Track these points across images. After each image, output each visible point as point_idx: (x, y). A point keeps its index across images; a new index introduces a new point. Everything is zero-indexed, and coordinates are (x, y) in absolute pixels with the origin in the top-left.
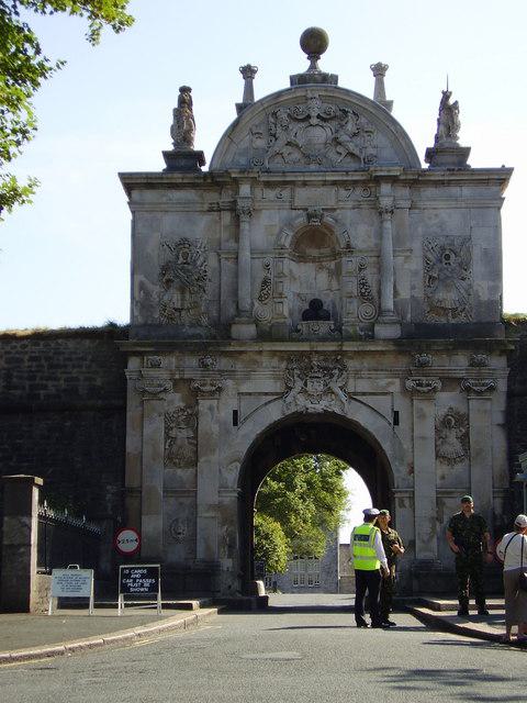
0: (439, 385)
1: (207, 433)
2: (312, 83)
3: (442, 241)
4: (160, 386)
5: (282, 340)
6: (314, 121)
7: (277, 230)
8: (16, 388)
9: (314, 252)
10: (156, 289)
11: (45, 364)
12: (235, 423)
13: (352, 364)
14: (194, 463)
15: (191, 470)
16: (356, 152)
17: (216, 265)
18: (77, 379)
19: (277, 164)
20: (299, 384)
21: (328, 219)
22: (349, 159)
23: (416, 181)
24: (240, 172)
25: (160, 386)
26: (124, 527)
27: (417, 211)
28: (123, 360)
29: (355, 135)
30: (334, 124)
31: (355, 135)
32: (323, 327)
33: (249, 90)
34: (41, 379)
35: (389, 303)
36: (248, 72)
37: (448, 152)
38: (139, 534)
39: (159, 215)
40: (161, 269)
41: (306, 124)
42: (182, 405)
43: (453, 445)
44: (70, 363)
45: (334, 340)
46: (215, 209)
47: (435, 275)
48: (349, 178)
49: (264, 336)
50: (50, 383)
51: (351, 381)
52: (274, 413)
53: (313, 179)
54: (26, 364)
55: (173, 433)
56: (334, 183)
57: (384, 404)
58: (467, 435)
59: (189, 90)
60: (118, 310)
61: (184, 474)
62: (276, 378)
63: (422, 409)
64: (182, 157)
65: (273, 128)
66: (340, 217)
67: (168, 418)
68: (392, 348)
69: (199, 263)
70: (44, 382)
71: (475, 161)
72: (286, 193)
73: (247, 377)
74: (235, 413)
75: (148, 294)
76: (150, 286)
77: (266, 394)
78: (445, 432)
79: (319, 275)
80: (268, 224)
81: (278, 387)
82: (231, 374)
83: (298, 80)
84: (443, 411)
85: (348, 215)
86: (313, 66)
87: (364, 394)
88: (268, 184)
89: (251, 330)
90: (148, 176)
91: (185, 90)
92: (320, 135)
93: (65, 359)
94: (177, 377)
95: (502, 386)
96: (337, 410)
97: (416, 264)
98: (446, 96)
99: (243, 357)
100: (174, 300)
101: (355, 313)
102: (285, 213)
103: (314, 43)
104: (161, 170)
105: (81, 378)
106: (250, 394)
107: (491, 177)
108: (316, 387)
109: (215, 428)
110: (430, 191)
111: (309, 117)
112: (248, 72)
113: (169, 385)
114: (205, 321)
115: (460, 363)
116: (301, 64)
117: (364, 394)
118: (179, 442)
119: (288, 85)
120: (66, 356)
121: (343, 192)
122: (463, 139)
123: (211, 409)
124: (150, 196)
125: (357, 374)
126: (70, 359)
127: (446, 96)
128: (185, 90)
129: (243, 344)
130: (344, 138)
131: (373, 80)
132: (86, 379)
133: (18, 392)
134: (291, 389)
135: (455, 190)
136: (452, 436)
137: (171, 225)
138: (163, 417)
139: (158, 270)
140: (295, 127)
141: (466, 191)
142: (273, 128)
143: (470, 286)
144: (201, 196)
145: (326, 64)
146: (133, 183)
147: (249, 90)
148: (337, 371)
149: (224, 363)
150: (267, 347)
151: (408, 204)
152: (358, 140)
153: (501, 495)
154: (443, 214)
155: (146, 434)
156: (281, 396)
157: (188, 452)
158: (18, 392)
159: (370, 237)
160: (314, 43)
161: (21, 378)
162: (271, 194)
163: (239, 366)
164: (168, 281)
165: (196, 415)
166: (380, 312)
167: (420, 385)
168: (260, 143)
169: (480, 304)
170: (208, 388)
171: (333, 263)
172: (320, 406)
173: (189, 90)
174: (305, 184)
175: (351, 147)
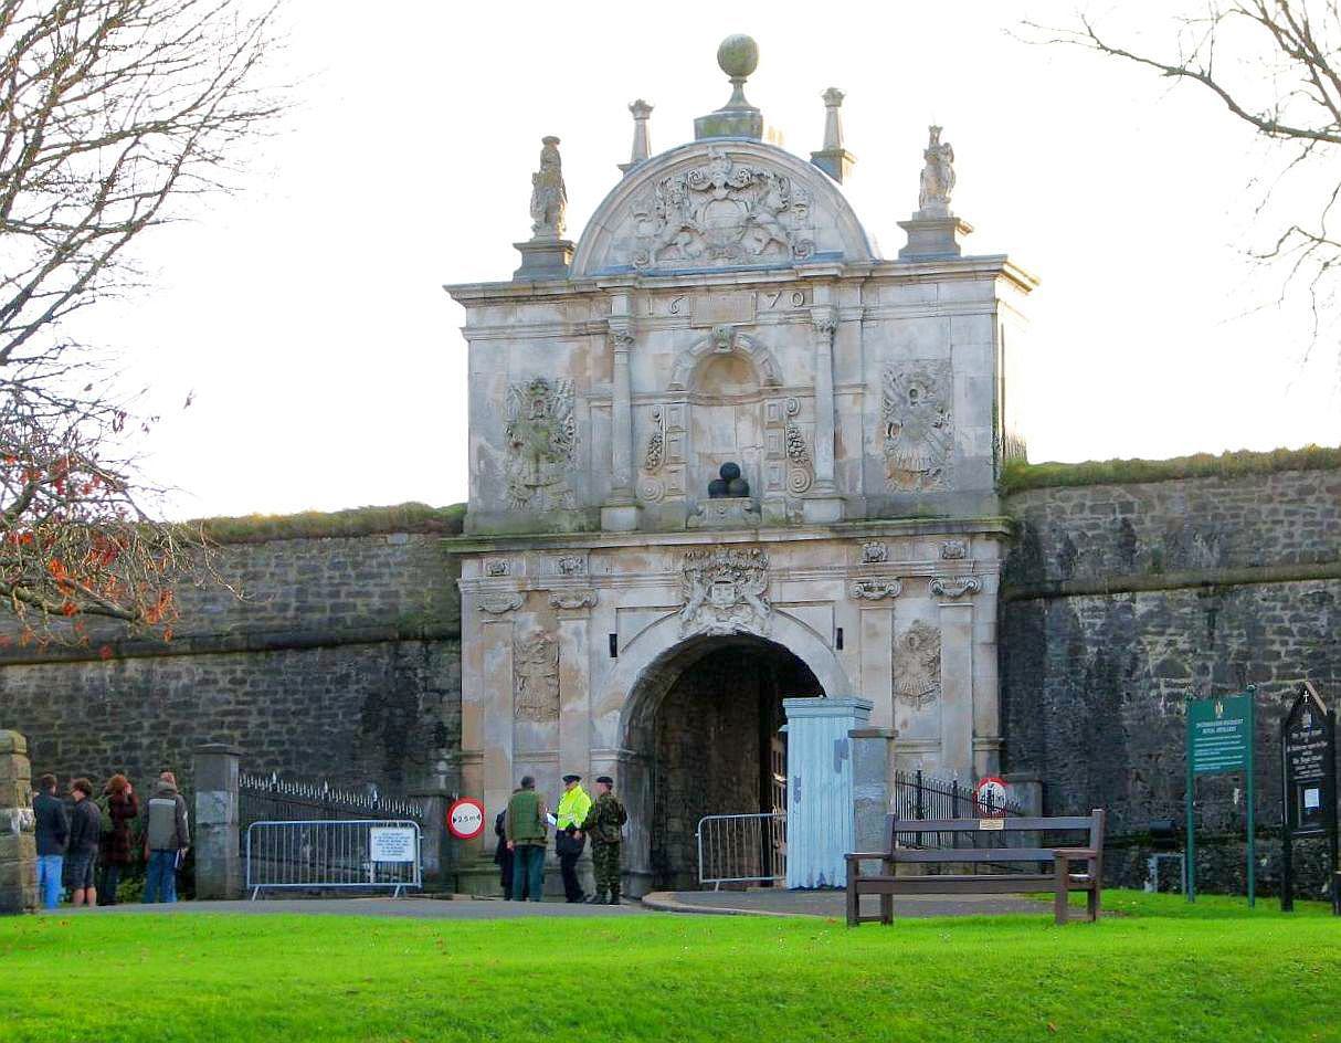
0: (896, 587)
1: (571, 669)
2: (734, 125)
3: (908, 369)
4: (505, 602)
5: (671, 530)
6: (721, 193)
7: (670, 362)
8: (311, 609)
9: (732, 389)
10: (501, 456)
11: (353, 574)
12: (614, 652)
13: (778, 561)
14: (556, 713)
15: (552, 724)
16: (781, 237)
17: (587, 418)
18: (396, 594)
19: (671, 262)
20: (699, 593)
21: (743, 344)
22: (773, 248)
23: (871, 276)
24: (610, 280)
25: (505, 602)
26: (463, 798)
27: (873, 323)
28: (456, 561)
29: (780, 211)
30: (747, 196)
31: (780, 211)
32: (735, 507)
33: (641, 139)
34: (349, 594)
35: (824, 468)
36: (641, 110)
37: (933, 233)
38: (482, 811)
39: (504, 344)
40: (523, 425)
41: (708, 197)
42: (538, 629)
43: (916, 674)
44: (386, 570)
45: (747, 527)
46: (582, 332)
47: (897, 422)
48: (771, 279)
49: (645, 526)
50: (359, 602)
51: (775, 587)
52: (668, 637)
53: (719, 282)
54: (326, 575)
55: (525, 670)
56: (751, 286)
57: (822, 618)
58: (937, 660)
59: (556, 141)
60: (444, 484)
61: (541, 729)
62: (670, 585)
63: (873, 626)
64: (544, 253)
65: (662, 206)
66: (760, 338)
67: (517, 648)
68: (829, 535)
69: (560, 416)
70: (351, 600)
71: (968, 246)
72: (683, 306)
73: (630, 582)
74: (613, 637)
75: (490, 464)
76: (494, 453)
77: (657, 608)
78: (907, 657)
79: (739, 425)
80: (665, 351)
81: (673, 598)
82: (606, 581)
83: (708, 127)
84: (905, 626)
85: (771, 336)
86: (738, 96)
87: (795, 604)
88: (656, 292)
89: (627, 515)
90: (504, 283)
91: (551, 142)
92: (727, 214)
93: (380, 565)
94: (529, 588)
95: (991, 584)
96: (755, 630)
97: (873, 405)
98: (935, 131)
99: (623, 555)
100: (526, 472)
101: (774, 484)
102: (681, 334)
103: (738, 60)
104: (509, 278)
105: (402, 592)
106: (634, 609)
107: (978, 268)
108: (722, 596)
109: (583, 662)
110: (892, 294)
111: (712, 187)
112: (641, 110)
113: (518, 600)
114: (570, 501)
115: (928, 554)
116: (716, 93)
117: (795, 604)
118: (533, 682)
119: (692, 139)
120: (382, 559)
121: (763, 298)
122: (959, 204)
123: (577, 633)
124: (493, 316)
125: (784, 575)
126: (388, 565)
127: (935, 131)
128: (551, 142)
129: (616, 538)
130: (763, 217)
131: (1266, 27)
132: (410, 594)
133: (317, 616)
134: (688, 600)
135: (928, 290)
136: (915, 662)
137: (521, 361)
138: (509, 649)
139: (504, 428)
140: (697, 201)
141: (946, 290)
142: (662, 206)
143: (949, 436)
144: (564, 314)
145: (756, 90)
146: (474, 297)
147: (641, 139)
148: (751, 572)
149: (598, 565)
150: (653, 541)
151: (858, 314)
152: (783, 219)
153: (986, 747)
154: (910, 328)
155: (484, 672)
156: (677, 610)
157: (544, 698)
158: (317, 616)
159: (803, 367)
160: (738, 60)
161: (319, 595)
162: (663, 307)
163: (617, 570)
164: (517, 445)
165: (557, 644)
166: (813, 481)
167: (869, 589)
168: (647, 228)
169: (964, 462)
170: (572, 603)
171: (758, 406)
172: (727, 627)
173: (556, 141)
174: (709, 289)
175: (774, 229)
